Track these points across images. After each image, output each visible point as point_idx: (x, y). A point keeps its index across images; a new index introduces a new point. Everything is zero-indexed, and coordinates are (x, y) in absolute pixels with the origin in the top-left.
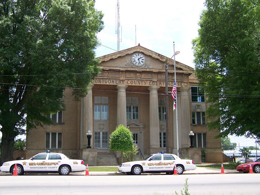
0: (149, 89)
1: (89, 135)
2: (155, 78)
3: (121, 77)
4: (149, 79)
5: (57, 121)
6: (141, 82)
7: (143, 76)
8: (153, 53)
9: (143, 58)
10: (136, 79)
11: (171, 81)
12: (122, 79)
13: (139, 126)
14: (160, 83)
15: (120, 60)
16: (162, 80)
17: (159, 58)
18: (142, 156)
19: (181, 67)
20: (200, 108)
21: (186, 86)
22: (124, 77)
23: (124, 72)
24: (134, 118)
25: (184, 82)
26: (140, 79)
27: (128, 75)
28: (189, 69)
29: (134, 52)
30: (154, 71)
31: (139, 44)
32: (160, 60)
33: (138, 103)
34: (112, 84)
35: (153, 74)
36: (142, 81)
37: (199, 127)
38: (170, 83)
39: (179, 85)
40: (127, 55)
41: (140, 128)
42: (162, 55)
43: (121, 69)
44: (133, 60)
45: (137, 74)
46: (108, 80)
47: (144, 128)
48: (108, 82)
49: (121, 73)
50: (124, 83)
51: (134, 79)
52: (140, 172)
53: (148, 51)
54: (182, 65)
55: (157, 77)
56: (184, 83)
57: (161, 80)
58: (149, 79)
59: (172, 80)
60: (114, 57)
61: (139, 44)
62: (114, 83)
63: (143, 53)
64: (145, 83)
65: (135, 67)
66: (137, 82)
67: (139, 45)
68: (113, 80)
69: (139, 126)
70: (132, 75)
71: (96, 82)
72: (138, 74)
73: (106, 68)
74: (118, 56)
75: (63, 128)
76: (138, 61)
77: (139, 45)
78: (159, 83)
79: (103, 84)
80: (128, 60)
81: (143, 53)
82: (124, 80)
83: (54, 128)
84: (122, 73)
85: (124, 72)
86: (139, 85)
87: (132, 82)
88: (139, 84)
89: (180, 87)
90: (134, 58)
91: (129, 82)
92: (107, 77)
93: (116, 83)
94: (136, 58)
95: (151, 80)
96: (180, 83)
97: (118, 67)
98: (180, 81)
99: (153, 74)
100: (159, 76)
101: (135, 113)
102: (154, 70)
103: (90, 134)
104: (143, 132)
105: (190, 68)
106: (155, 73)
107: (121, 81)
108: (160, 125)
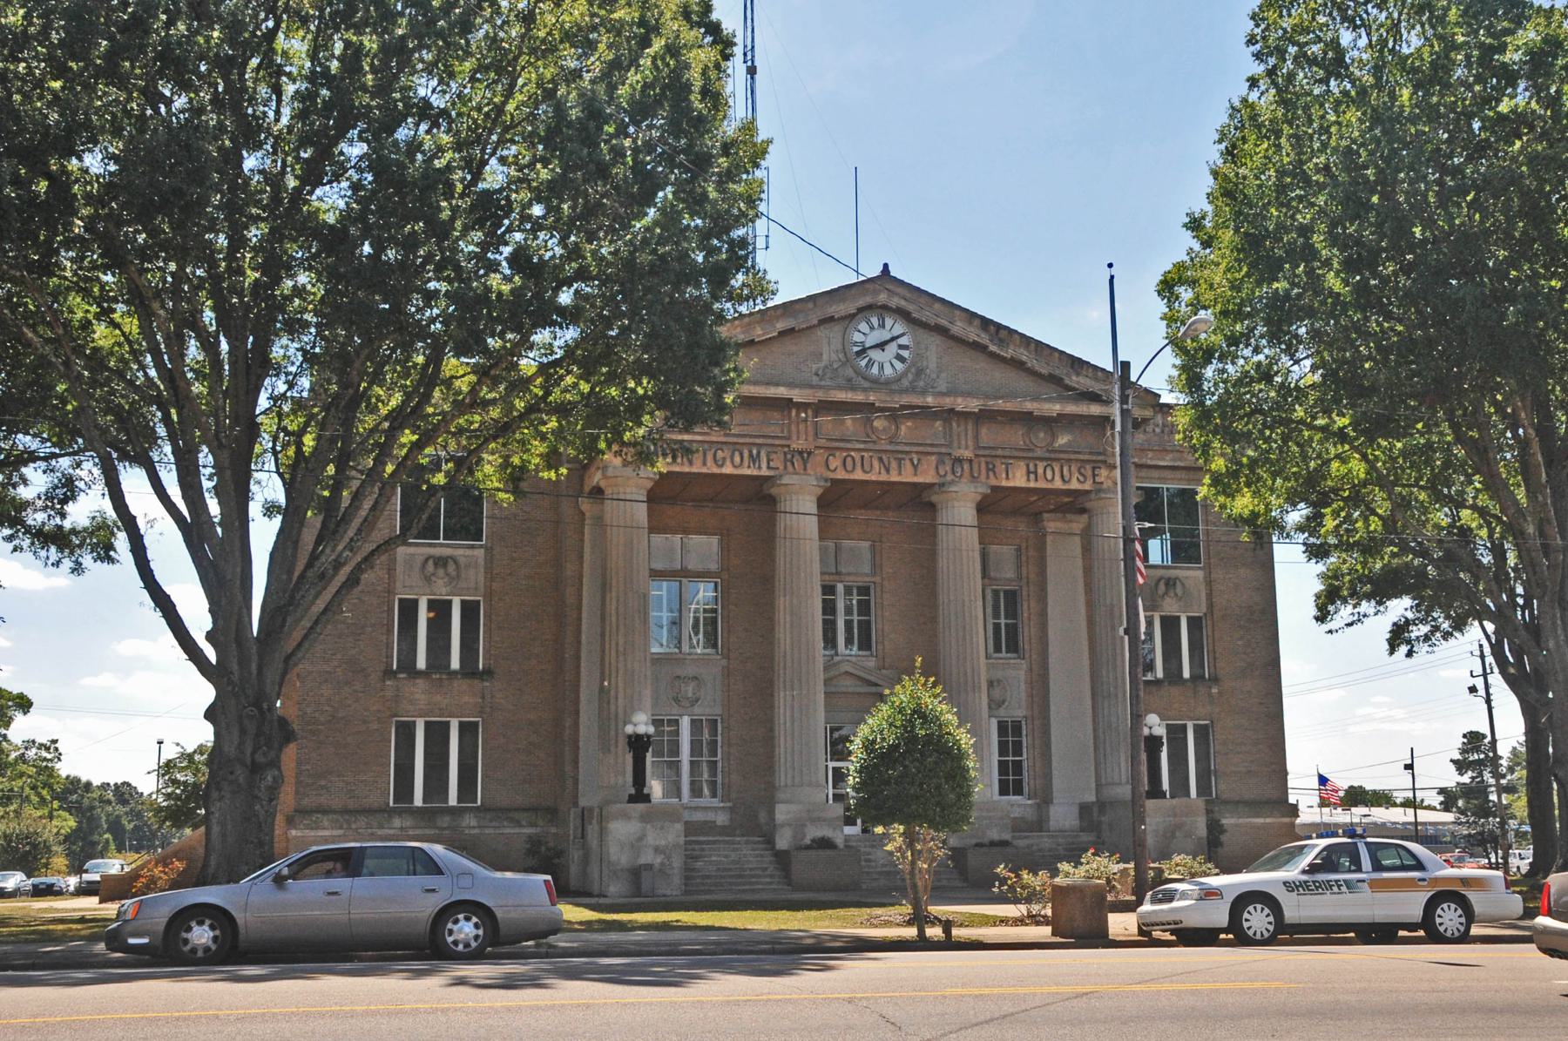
0: (774, 491)
5: (455, 664)
6: (894, 464)
9: (904, 341)
11: (1041, 459)
12: (798, 444)
14: (991, 469)
15: (789, 345)
16: (1000, 452)
17: (984, 339)
29: (861, 310)
31: (886, 266)
32: (993, 348)
33: (867, 569)
37: (1175, 691)
38: (1040, 471)
43: (797, 395)
46: (727, 453)
48: (728, 462)
52: (1271, 928)
55: (976, 437)
61: (886, 266)
64: (915, 467)
65: (866, 384)
66: (876, 464)
74: (781, 325)
75: (483, 697)
76: (886, 349)
78: (983, 466)
79: (704, 470)
80: (828, 344)
82: (809, 453)
83: (438, 698)
86: (884, 477)
88: (888, 471)
89: (1087, 486)
93: (769, 468)
95: (943, 450)
96: (1089, 467)
98: (1087, 457)
101: (1003, 621)
103: (642, 729)
107: (797, 457)
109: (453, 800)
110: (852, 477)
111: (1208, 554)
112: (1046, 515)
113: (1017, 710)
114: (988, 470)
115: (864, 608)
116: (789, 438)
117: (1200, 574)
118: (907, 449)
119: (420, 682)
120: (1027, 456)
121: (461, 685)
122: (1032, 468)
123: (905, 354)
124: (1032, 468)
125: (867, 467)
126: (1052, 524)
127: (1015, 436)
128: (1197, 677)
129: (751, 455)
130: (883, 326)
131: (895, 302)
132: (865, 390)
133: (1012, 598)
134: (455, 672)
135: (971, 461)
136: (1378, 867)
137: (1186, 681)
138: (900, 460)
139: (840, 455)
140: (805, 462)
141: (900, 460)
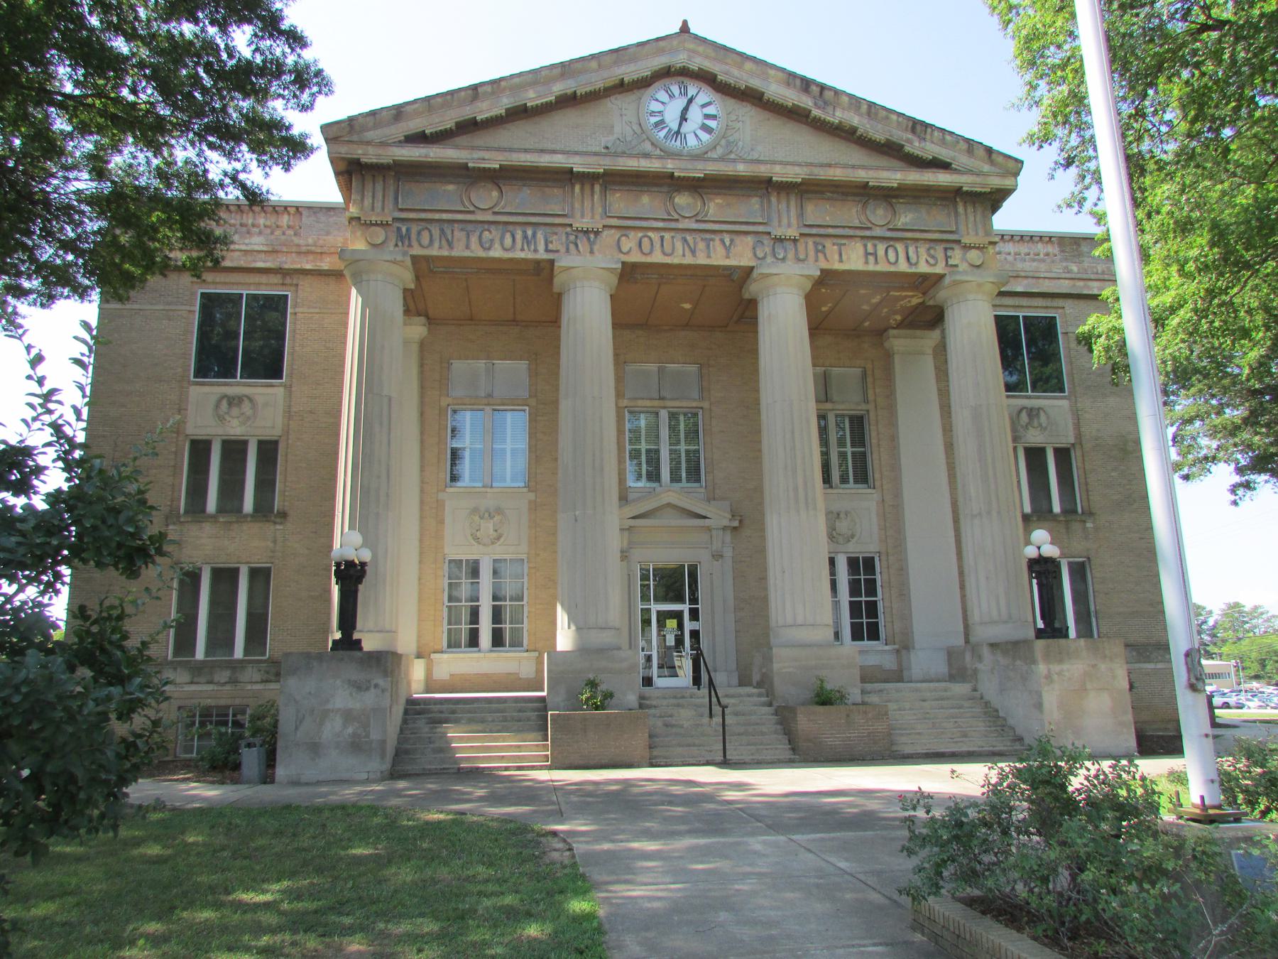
1: (350, 564)
2: (785, 221)
3: (578, 215)
4: (751, 228)
6: (701, 245)
7: (716, 207)
8: (772, 72)
9: (711, 110)
10: (673, 225)
13: (705, 517)
14: (821, 250)
17: (806, 102)
18: (714, 699)
19: (944, 154)
20: (1040, 425)
21: (978, 267)
22: (597, 217)
23: (597, 188)
24: (675, 478)
25: (965, 240)
26: (695, 226)
27: (620, 202)
28: (992, 163)
30: (781, 173)
31: (685, 23)
32: (816, 112)
33: (696, 395)
34: (523, 255)
35: (774, 199)
36: (708, 236)
38: (881, 252)
39: (932, 261)
40: (622, 87)
41: (709, 529)
42: (823, 88)
43: (579, 164)
44: (653, 120)
45: (676, 200)
46: (495, 233)
47: (735, 528)
48: (497, 245)
49: (577, 188)
50: (596, 248)
51: (660, 225)
53: (740, 67)
54: (948, 138)
55: (801, 215)
56: (967, 248)
57: (822, 231)
58: (751, 228)
59: (889, 234)
60: (532, 97)
61: (685, 23)
62: (536, 251)
63: (709, 79)
64: (727, 249)
66: (679, 245)
67: (685, 28)
68: (530, 233)
69: (705, 517)
70: (647, 203)
71: (426, 241)
72: (682, 200)
73: (486, 155)
74: (559, 88)
75: (275, 542)
76: (687, 124)
77: (685, 28)
79: (467, 254)
80: (619, 113)
81: (709, 79)
82: (597, 233)
84: (582, 189)
85: (597, 188)
86: (689, 260)
87: (646, 241)
88: (693, 252)
89: (939, 269)
90: (655, 106)
91: (627, 244)
92: (495, 213)
93: (547, 250)
94: (665, 105)
95: (761, 229)
97: (554, 152)
99: (774, 199)
100: (810, 208)
102: (778, 169)
104: (728, 553)
105: (1000, 159)
106: (786, 188)
108: (828, 513)
109: (239, 652)
110: (649, 260)
111: (1072, 382)
112: (892, 332)
113: (866, 545)
114: (817, 251)
115: (693, 435)
116: (573, 216)
117: (1065, 403)
118: (716, 227)
119: (208, 528)
120: (864, 235)
121: (255, 528)
122: (870, 249)
123: (712, 124)
124: (870, 249)
125: (667, 248)
126: (899, 342)
127: (849, 214)
128: (1069, 510)
129: (525, 237)
130: (705, 128)
131: (696, 63)
132: (660, 158)
133: (858, 424)
134: (247, 516)
135: (795, 241)
136: (663, 617)
137: (1056, 515)
138: (708, 242)
139: (635, 236)
140: (592, 244)
141: (708, 242)
